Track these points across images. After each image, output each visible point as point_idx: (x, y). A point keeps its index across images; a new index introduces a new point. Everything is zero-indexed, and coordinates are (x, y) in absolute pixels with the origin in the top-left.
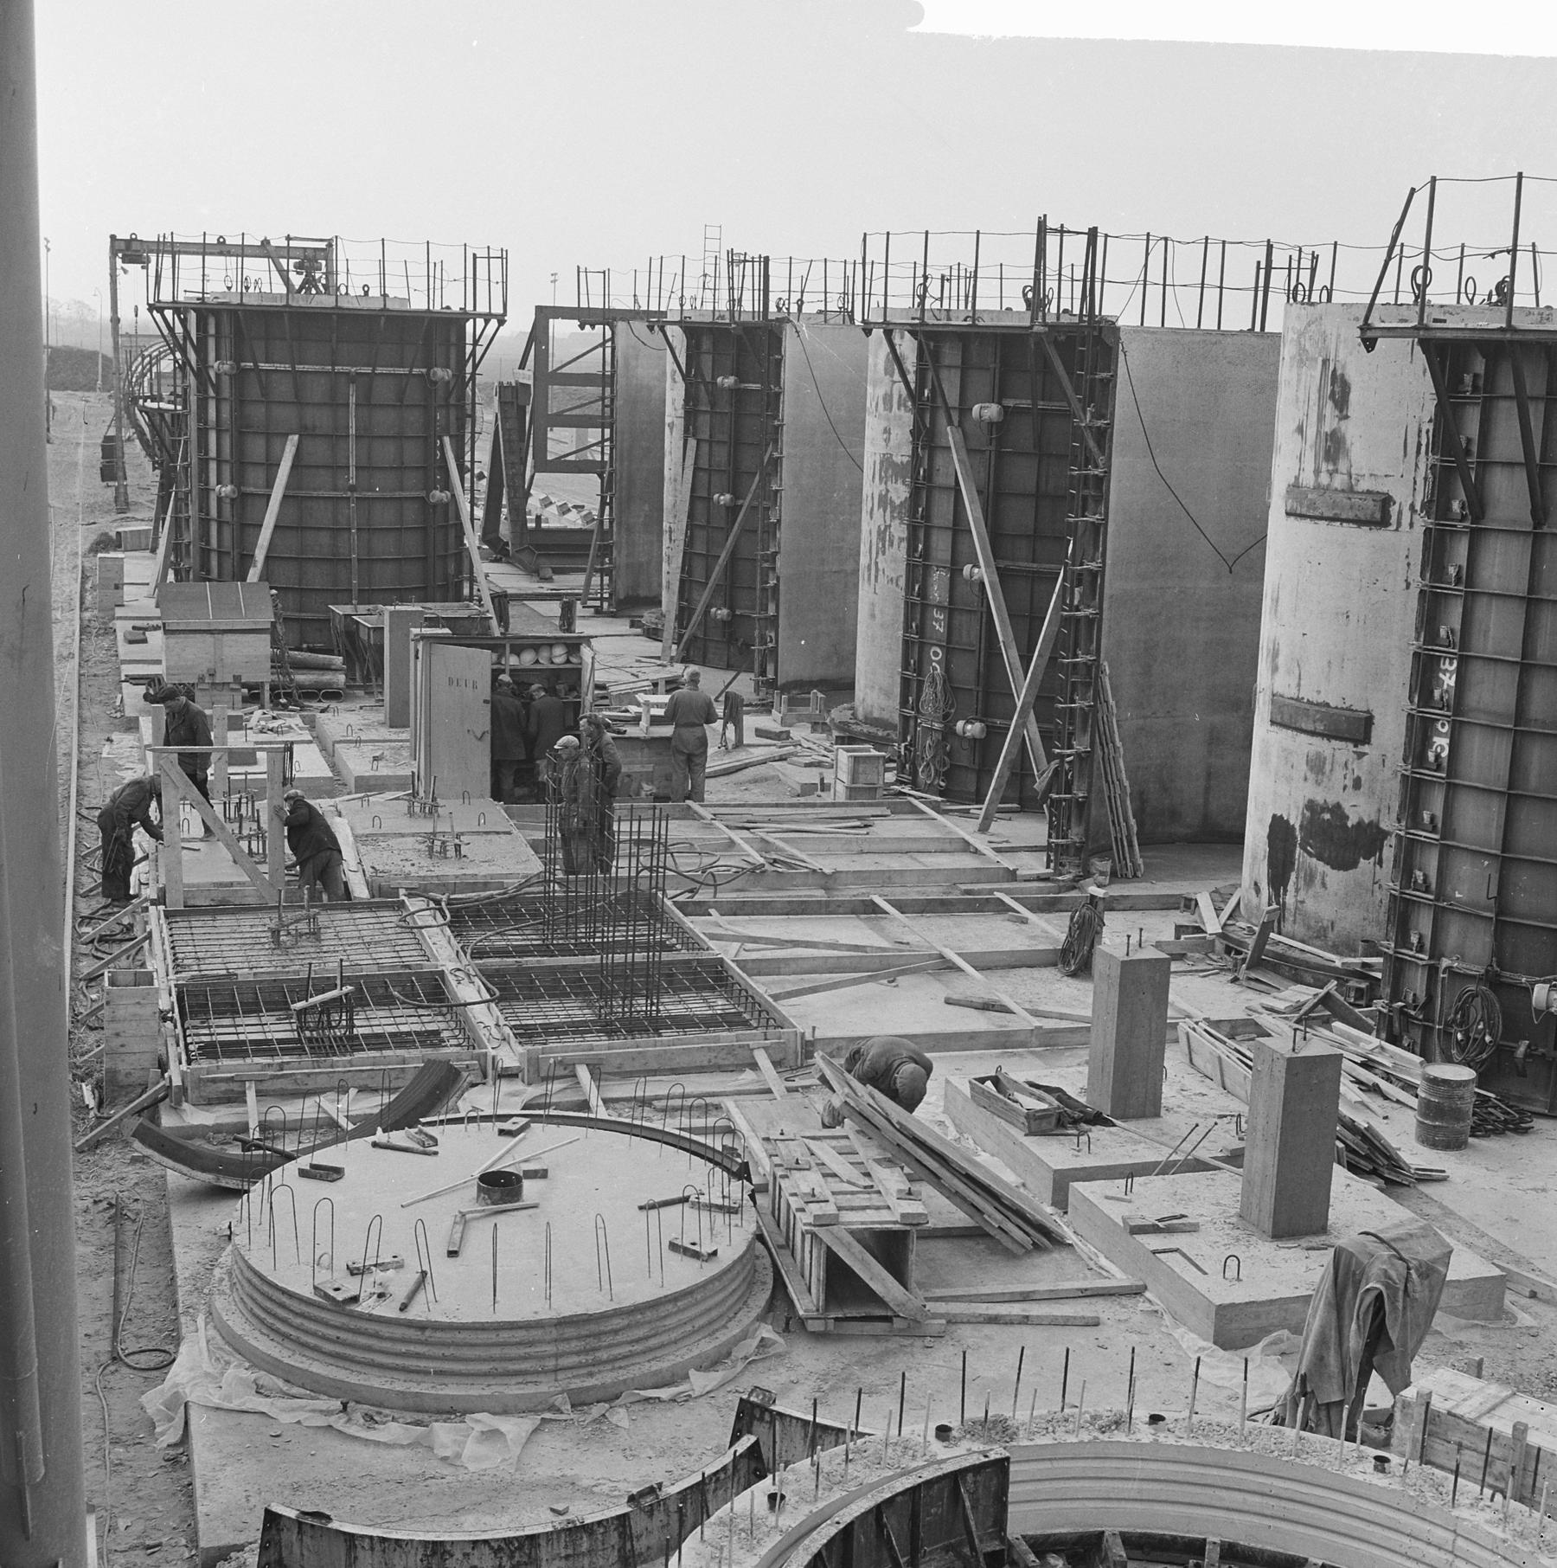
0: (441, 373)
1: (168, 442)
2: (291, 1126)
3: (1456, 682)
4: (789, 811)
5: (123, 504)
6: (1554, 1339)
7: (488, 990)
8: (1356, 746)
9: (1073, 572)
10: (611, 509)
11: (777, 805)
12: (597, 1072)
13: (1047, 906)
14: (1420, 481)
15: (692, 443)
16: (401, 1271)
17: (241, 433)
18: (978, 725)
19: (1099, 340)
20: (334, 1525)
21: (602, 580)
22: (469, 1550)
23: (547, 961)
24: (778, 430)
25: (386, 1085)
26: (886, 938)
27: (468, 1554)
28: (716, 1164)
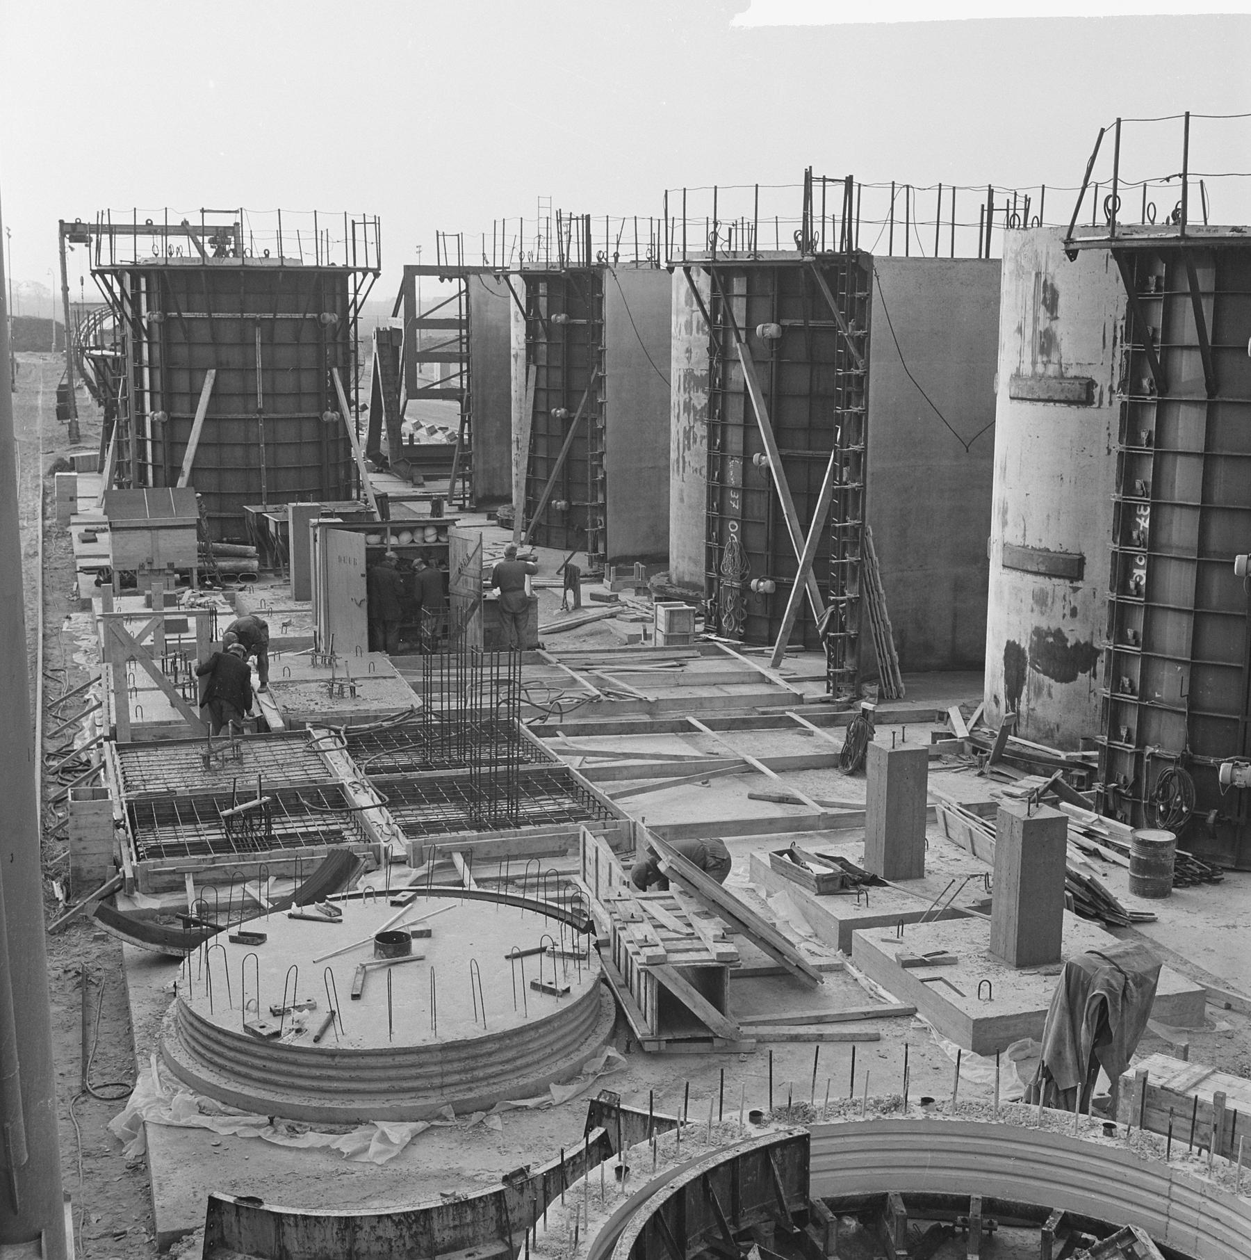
0: (330, 317)
1: (110, 383)
2: (222, 908)
3: (1150, 525)
4: (619, 655)
5: (75, 437)
6: (1246, 1040)
7: (380, 797)
8: (1072, 582)
9: (842, 453)
10: (469, 426)
11: (609, 651)
12: (469, 856)
13: (828, 722)
14: (1117, 367)
15: (533, 368)
16: (315, 1011)
17: (169, 370)
18: (768, 582)
19: (856, 266)
20: (266, 1207)
21: (464, 485)
22: (375, 1224)
23: (427, 774)
24: (601, 354)
25: (299, 873)
26: (700, 750)
27: (375, 1227)
28: (568, 923)
